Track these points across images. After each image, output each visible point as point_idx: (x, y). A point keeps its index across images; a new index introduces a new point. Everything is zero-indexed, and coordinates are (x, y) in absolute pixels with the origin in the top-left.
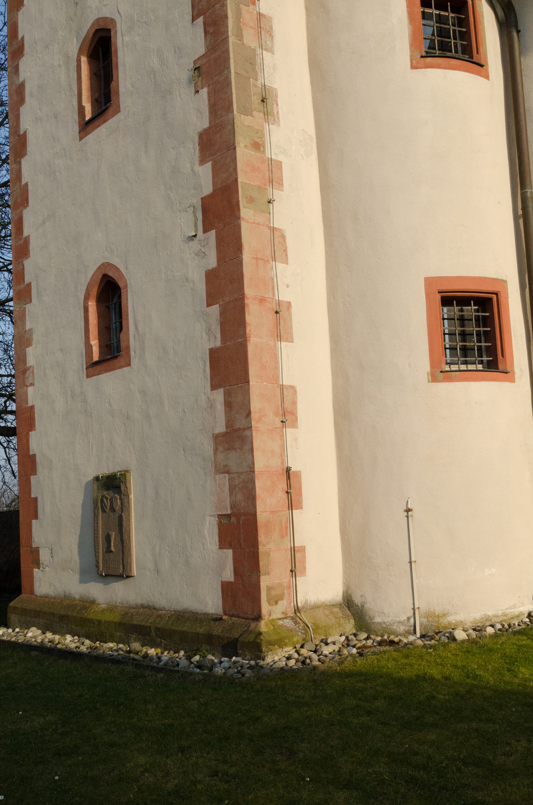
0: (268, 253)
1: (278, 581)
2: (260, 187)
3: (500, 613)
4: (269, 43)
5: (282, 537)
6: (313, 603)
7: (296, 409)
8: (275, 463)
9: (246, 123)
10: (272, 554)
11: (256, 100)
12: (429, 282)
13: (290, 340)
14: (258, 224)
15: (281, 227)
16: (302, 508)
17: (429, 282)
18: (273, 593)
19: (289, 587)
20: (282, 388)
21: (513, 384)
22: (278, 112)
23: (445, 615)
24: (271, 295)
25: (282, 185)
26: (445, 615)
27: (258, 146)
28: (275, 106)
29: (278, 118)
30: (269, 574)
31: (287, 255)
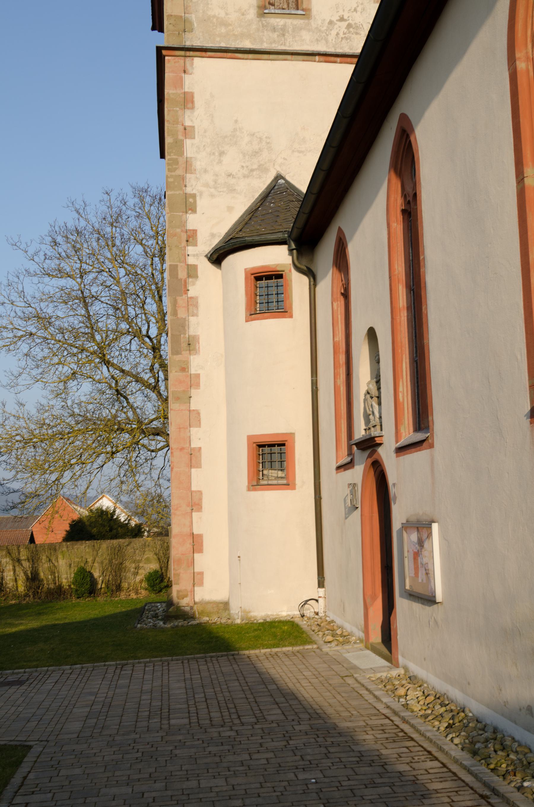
0: (188, 424)
1: (184, 588)
2: (184, 391)
3: (275, 613)
4: (195, 312)
5: (189, 567)
6: (207, 600)
7: (201, 502)
8: (186, 530)
9: (177, 359)
10: (181, 575)
11: (184, 345)
12: (249, 437)
13: (199, 466)
14: (182, 410)
15: (197, 409)
16: (202, 552)
17: (249, 437)
18: (181, 594)
19: (191, 592)
20: (192, 492)
21: (294, 491)
22: (199, 348)
23: (250, 612)
24: (188, 445)
25: (199, 386)
26: (250, 612)
27: (184, 369)
28: (197, 344)
29: (199, 351)
30: (179, 584)
31: (200, 423)
